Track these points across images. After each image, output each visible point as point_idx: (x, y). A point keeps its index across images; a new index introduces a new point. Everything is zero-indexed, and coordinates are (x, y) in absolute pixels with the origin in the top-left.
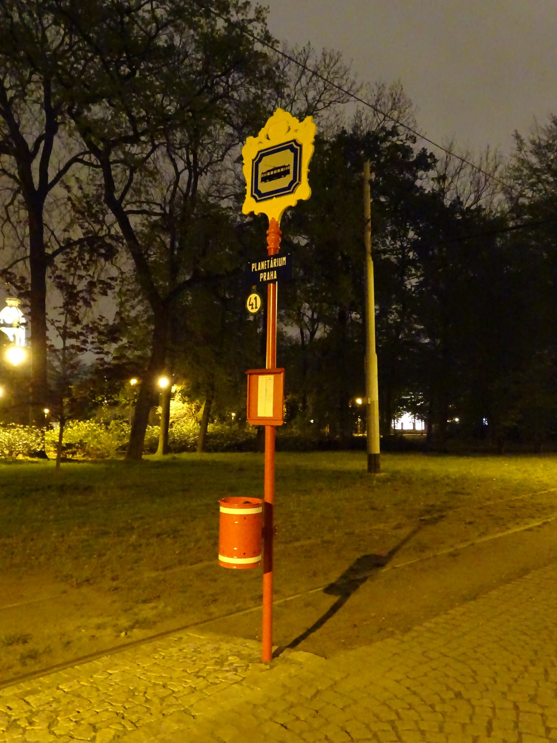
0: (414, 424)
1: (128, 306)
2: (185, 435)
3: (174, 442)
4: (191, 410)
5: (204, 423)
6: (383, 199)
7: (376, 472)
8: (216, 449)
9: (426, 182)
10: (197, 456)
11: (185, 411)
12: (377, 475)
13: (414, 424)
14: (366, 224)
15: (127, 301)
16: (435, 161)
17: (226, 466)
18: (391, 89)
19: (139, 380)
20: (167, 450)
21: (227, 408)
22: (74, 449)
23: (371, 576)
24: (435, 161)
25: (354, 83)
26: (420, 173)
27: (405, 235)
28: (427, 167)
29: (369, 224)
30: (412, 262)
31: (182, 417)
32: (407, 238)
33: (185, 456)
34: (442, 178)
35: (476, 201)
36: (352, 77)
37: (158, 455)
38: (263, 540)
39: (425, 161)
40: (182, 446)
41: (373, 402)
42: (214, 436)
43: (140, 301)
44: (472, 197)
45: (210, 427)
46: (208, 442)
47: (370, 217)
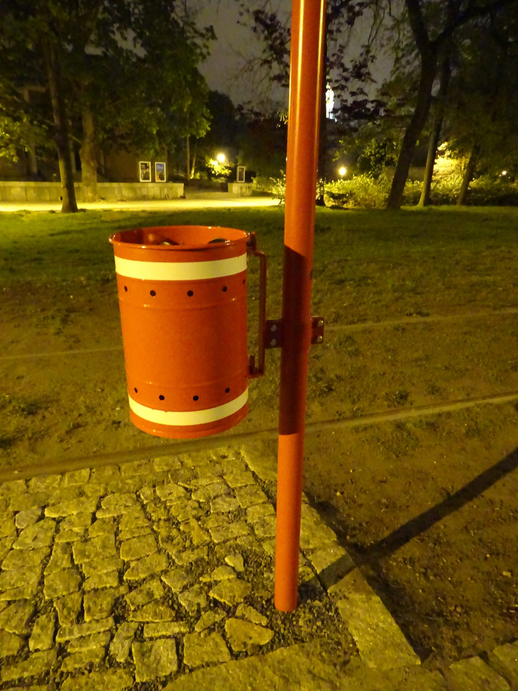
1: (403, 61)
2: (448, 190)
3: (436, 195)
4: (461, 167)
5: (468, 178)
6: (69, 37)
8: (477, 203)
10: (459, 208)
11: (453, 168)
15: (403, 56)
17: (486, 219)
20: (428, 201)
21: (207, 158)
22: (345, 199)
31: (450, 174)
33: (444, 208)
37: (420, 206)
38: (129, 216)
40: (445, 199)
42: (475, 190)
43: (417, 56)
45: (473, 183)
46: (468, 196)
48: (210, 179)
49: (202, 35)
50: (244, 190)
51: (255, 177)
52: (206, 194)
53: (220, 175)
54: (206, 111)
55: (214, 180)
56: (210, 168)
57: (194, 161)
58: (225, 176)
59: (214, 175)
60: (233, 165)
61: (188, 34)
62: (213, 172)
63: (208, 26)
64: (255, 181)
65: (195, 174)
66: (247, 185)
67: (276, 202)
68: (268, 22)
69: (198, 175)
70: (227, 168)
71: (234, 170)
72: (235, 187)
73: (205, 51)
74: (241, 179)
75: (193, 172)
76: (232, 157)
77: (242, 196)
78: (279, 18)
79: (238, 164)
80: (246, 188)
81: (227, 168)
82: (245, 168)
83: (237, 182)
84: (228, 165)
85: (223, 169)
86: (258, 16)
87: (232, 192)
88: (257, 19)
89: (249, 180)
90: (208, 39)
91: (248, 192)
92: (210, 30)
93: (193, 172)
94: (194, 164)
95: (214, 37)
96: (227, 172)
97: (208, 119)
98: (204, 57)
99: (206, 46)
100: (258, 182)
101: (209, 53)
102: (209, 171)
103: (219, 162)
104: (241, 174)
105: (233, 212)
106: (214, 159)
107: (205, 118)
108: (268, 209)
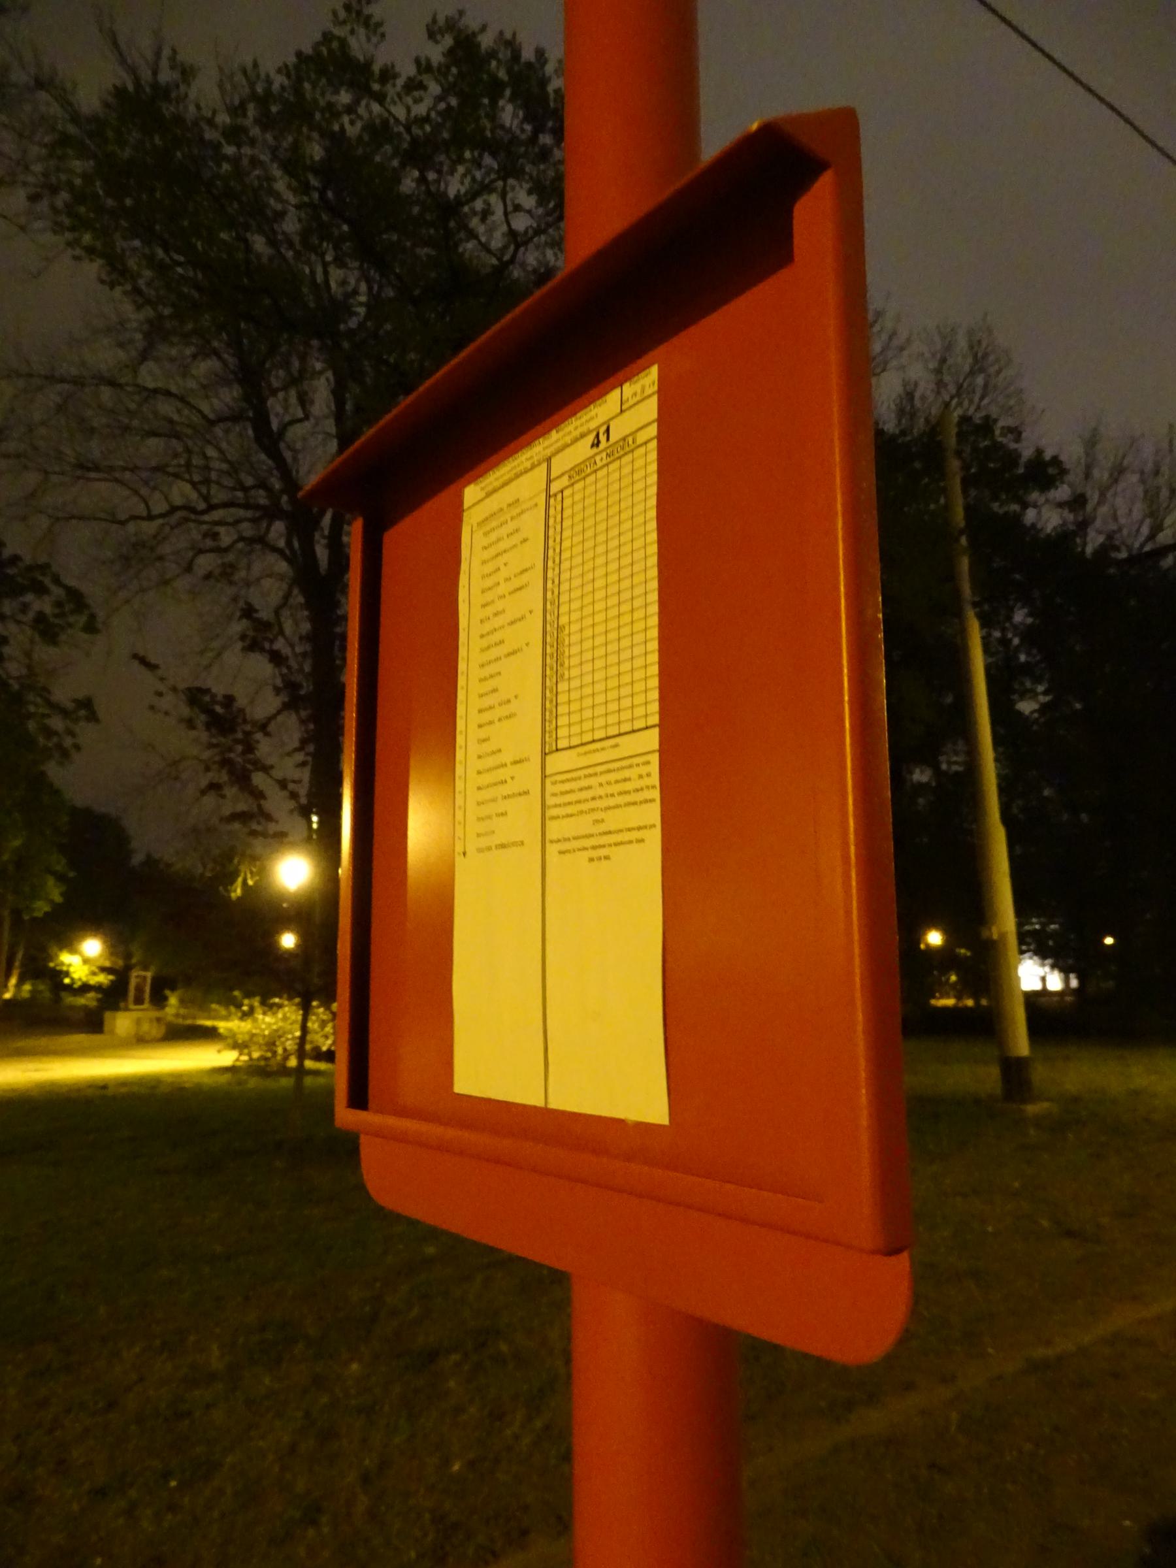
0: (1043, 979)
7: (1024, 1101)
9: (1046, 515)
12: (1031, 1109)
13: (1043, 979)
14: (957, 540)
16: (1063, 472)
18: (970, 333)
19: (298, 946)
23: (331, 461)
24: (1063, 472)
25: (893, 335)
26: (1035, 496)
27: (1009, 618)
28: (1047, 484)
29: (964, 541)
30: (1026, 669)
32: (1011, 623)
34: (1078, 502)
35: (1152, 537)
36: (889, 325)
39: (1044, 472)
41: (1003, 936)
44: (1145, 530)
47: (962, 524)
48: (57, 1000)
49: (65, 713)
50: (146, 1027)
51: (173, 989)
52: (43, 1042)
53: (85, 988)
54: (60, 863)
55: (70, 1000)
56: (61, 972)
57: (20, 955)
58: (98, 988)
59: (69, 988)
60: (120, 963)
61: (32, 709)
62: (67, 981)
63: (80, 695)
64: (173, 1000)
65: (19, 985)
66: (155, 1014)
67: (228, 1058)
68: (218, 709)
69: (27, 987)
70: (103, 969)
71: (121, 976)
72: (122, 1022)
73: (68, 742)
74: (139, 1000)
75: (13, 981)
76: (118, 944)
77: (141, 1041)
78: (241, 702)
79: (134, 961)
80: (151, 1020)
81: (103, 969)
82: (149, 975)
83: (127, 1009)
84: (107, 964)
85: (94, 974)
86: (195, 696)
87: (112, 1032)
88: (971, 347)
89: (159, 1000)
90: (76, 720)
91: (157, 1031)
92: (86, 704)
93: (13, 981)
94: (17, 964)
95: (93, 717)
96: (103, 979)
97: (61, 878)
98: (65, 754)
99: (72, 734)
100: (182, 1002)
101: (77, 747)
102: (56, 976)
103: (85, 958)
104: (140, 990)
105: (114, 1098)
106: (73, 950)
107: (54, 873)
108: (207, 1081)
